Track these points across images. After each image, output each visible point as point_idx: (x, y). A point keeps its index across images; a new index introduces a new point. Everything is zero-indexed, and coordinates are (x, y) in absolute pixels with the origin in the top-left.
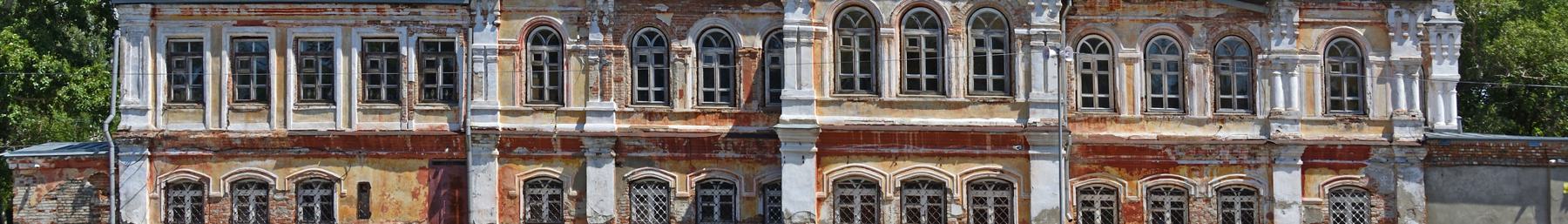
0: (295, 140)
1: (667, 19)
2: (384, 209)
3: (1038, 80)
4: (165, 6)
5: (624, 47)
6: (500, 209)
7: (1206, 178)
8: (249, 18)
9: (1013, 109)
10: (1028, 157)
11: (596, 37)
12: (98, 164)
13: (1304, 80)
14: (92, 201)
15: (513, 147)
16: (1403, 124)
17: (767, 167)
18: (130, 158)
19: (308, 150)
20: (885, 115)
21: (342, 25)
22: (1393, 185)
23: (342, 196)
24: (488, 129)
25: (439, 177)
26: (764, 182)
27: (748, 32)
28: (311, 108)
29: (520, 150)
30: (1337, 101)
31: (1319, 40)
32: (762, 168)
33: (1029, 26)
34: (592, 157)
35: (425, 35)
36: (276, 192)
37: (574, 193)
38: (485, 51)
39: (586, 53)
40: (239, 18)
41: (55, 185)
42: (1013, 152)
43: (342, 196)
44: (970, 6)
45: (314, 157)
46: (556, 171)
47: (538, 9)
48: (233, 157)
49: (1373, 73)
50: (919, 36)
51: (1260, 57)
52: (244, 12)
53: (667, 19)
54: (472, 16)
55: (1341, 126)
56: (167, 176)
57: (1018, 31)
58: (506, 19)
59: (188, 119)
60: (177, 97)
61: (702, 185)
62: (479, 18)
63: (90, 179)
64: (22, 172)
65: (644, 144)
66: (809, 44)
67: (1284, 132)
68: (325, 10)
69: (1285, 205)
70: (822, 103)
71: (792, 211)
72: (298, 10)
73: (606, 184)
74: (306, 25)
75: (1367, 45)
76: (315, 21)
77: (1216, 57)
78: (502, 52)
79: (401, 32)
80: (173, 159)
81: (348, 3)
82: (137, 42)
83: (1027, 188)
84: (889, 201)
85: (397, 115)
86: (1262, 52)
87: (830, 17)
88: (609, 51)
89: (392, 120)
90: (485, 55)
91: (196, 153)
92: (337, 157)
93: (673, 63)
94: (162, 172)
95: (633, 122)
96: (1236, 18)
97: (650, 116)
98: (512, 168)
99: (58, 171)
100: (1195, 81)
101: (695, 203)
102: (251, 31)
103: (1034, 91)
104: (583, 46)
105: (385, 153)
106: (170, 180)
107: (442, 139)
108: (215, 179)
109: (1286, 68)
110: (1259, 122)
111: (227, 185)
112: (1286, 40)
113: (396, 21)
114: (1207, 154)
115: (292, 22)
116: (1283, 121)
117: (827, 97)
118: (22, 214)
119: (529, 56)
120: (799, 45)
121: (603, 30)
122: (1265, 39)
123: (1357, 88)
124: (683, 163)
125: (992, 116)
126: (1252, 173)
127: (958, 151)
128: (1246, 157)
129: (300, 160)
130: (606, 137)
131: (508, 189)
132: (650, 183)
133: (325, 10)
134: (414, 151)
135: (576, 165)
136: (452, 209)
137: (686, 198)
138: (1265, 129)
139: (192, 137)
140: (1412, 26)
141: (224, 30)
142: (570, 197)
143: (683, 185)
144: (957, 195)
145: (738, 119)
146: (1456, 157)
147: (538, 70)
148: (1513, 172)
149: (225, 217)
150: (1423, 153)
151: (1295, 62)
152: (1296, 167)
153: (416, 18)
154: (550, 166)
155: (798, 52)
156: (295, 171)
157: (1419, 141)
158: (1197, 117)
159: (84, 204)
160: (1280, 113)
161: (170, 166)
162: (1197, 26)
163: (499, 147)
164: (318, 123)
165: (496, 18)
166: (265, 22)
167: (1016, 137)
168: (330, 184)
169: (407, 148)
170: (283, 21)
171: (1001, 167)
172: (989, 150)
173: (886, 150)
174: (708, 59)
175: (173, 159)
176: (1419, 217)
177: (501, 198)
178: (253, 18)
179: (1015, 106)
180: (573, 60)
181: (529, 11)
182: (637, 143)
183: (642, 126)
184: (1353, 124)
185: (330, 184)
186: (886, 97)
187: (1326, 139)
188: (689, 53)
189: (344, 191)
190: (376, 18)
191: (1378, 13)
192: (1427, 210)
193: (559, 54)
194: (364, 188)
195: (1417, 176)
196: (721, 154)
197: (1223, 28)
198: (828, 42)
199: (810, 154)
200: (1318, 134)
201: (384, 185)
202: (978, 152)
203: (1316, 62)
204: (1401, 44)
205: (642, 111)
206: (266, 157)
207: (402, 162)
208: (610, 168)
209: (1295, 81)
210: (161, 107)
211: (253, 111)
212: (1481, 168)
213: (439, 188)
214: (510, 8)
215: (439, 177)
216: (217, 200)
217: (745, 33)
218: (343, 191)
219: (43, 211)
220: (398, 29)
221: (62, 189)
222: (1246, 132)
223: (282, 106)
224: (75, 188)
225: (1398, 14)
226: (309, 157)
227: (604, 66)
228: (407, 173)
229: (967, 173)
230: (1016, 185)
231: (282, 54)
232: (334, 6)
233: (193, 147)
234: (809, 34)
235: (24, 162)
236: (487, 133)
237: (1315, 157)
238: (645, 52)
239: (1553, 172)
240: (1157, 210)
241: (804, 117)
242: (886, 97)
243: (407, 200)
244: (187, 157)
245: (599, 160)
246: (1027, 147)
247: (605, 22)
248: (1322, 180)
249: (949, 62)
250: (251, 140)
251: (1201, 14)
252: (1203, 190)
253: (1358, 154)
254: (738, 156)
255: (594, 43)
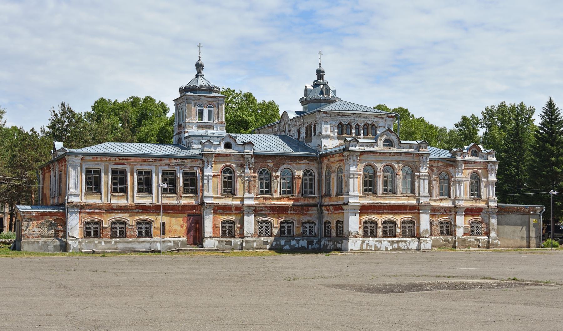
0: (138, 207)
1: (271, 165)
2: (170, 231)
3: (422, 190)
4: (87, 156)
5: (256, 174)
6: (213, 232)
7: (437, 218)
8: (119, 162)
9: (414, 198)
10: (419, 213)
11: (247, 171)
12: (59, 214)
13: (464, 187)
14: (55, 228)
15: (218, 210)
16: (492, 201)
17: (304, 216)
18: (72, 213)
19: (141, 210)
20: (378, 200)
21: (155, 165)
22: (488, 220)
23: (154, 227)
24: (210, 203)
25: (191, 220)
26: (303, 221)
27: (299, 169)
28: (143, 195)
29: (219, 211)
30: (473, 193)
31: (469, 173)
32: (303, 217)
33: (419, 172)
34: (246, 213)
35: (186, 169)
36: (129, 225)
37: (239, 226)
38: (208, 176)
39: (244, 177)
40: (115, 162)
41: (40, 222)
42: (415, 212)
43: (154, 227)
44: (403, 165)
45: (144, 213)
46: (233, 218)
47: (227, 161)
48: (112, 213)
49: (483, 185)
50: (387, 175)
51: (452, 179)
52: (117, 160)
53: (271, 165)
54: (203, 163)
55: (474, 201)
56: (86, 219)
57: (416, 174)
58: (215, 164)
59: (94, 198)
60: (88, 190)
61: (282, 223)
62: (206, 164)
63: (55, 220)
64: (26, 217)
65: (264, 209)
66: (357, 178)
67: (459, 204)
68: (149, 160)
69: (459, 227)
70: (360, 197)
71: (352, 231)
72: (139, 160)
73: (251, 223)
74: (141, 165)
75: (481, 175)
76: (145, 164)
77: (440, 179)
78: (214, 176)
79: (177, 169)
80: (88, 213)
81: (159, 158)
82: (75, 169)
83: (419, 223)
84: (380, 228)
85: (176, 198)
86: (453, 178)
87: (362, 169)
88: (252, 176)
89: (173, 200)
90: (208, 177)
91: (98, 211)
92: (153, 213)
93: (273, 181)
94: (84, 218)
95: (259, 201)
96: (446, 166)
97: (265, 199)
98: (217, 217)
99: (41, 217)
100: (434, 187)
101: (280, 229)
102: (120, 167)
103: (421, 193)
104: (243, 175)
105: (171, 212)
106: (87, 221)
107: (193, 207)
108: (105, 221)
109: (460, 183)
110: (452, 200)
111: (110, 223)
112: (460, 174)
113: (176, 164)
114: (437, 211)
115: (136, 164)
116: (459, 200)
117: (361, 195)
118: (26, 233)
119: (222, 178)
120: (354, 178)
121: (250, 169)
122: (454, 173)
123: (479, 190)
124: (276, 215)
125: (409, 201)
126: (450, 217)
127: (399, 212)
128: (448, 212)
129: (139, 214)
130: (251, 206)
131: (216, 225)
132: (264, 222)
133: (149, 160)
134: (181, 211)
135: (240, 216)
136: (196, 231)
137: (277, 227)
138: (454, 203)
139: (97, 205)
140: (494, 170)
141: (110, 166)
142: (237, 227)
143: (276, 222)
144: (399, 226)
145: (296, 200)
146: (505, 212)
147: (225, 183)
148: (520, 216)
149: (109, 234)
150: (497, 210)
151: (462, 181)
152: (462, 215)
153: (183, 163)
154: (231, 216)
155: (354, 180)
156: (137, 218)
157: (496, 206)
158: (434, 199)
159: (52, 229)
160: (458, 197)
161: (87, 216)
162: (435, 169)
163: (213, 210)
164: (146, 201)
165: (212, 164)
166: (126, 163)
167: (416, 207)
168: (150, 223)
169: (179, 210)
170: (133, 163)
171: (411, 217)
172: (408, 211)
173: (379, 212)
174: (284, 179)
175: (88, 213)
176: (495, 231)
177: (213, 227)
178: (121, 162)
179: (415, 197)
180: (239, 179)
181: (223, 162)
182: (261, 208)
183: (262, 202)
184: (478, 201)
185: (150, 223)
186: (379, 195)
187: (470, 206)
188: (279, 177)
189: (155, 225)
190: (167, 163)
191: (485, 165)
192: (498, 228)
193: (233, 177)
194: (163, 224)
195: (495, 218)
196: (289, 212)
197: (442, 170)
198: (361, 177)
199: (358, 213)
200: (468, 204)
201: (170, 223)
202: (405, 212)
203: (468, 181)
204: (491, 175)
205: (263, 197)
206: (125, 213)
207: (177, 215)
208: (252, 217)
209: (462, 187)
210: (84, 194)
211: (120, 196)
212: (512, 215)
213: (191, 224)
214: (217, 161)
215: (191, 220)
216: (106, 228)
217: (298, 170)
218: (155, 225)
219: (35, 232)
220: (176, 167)
221: (43, 223)
222: (447, 204)
223: (132, 194)
224: (48, 223)
225: (491, 166)
226: (142, 213)
227: (250, 181)
228: (179, 218)
229: (402, 219)
230: (415, 222)
231: (132, 175)
232: (153, 158)
233: (97, 209)
234: (357, 174)
235: (28, 213)
236: (210, 205)
237: (469, 212)
238: (263, 177)
239: (531, 216)
240: (114, 230)
241: (356, 201)
242: (379, 195)
243: (179, 228)
244: (94, 212)
245: (249, 214)
246: (419, 210)
247: (251, 166)
248: (470, 219)
249: (397, 184)
250: (120, 207)
251: (436, 165)
252: (436, 223)
253: (479, 210)
254: (295, 212)
255: (247, 173)
